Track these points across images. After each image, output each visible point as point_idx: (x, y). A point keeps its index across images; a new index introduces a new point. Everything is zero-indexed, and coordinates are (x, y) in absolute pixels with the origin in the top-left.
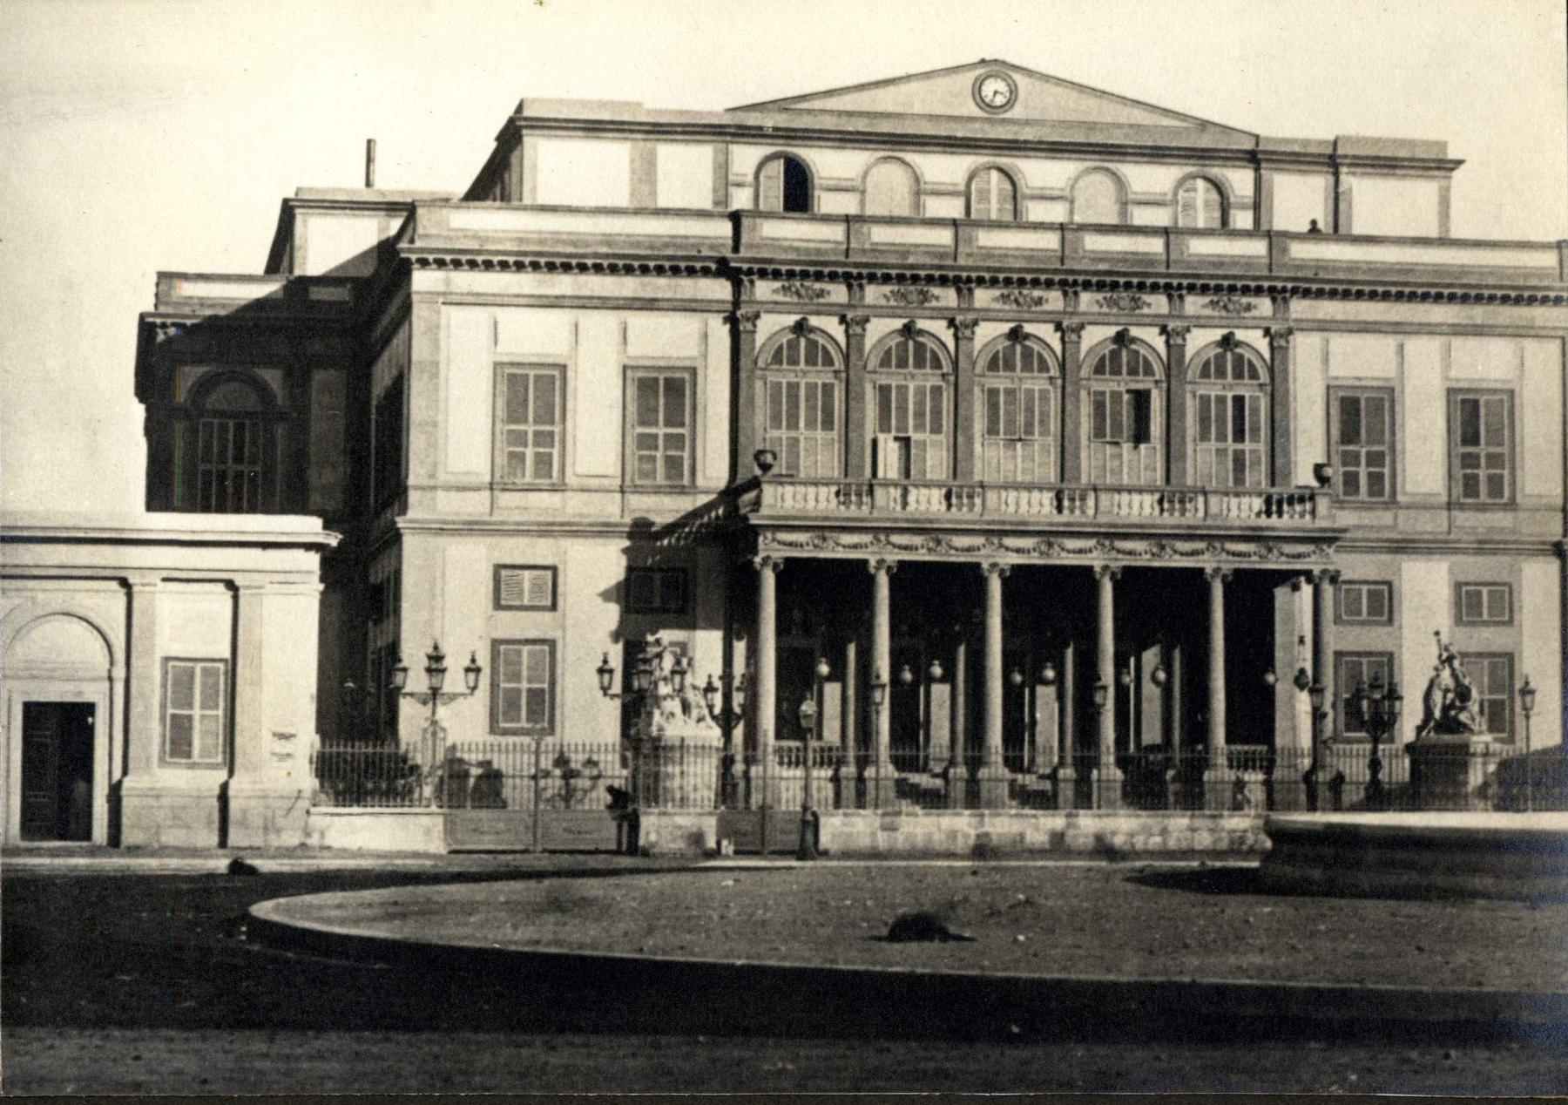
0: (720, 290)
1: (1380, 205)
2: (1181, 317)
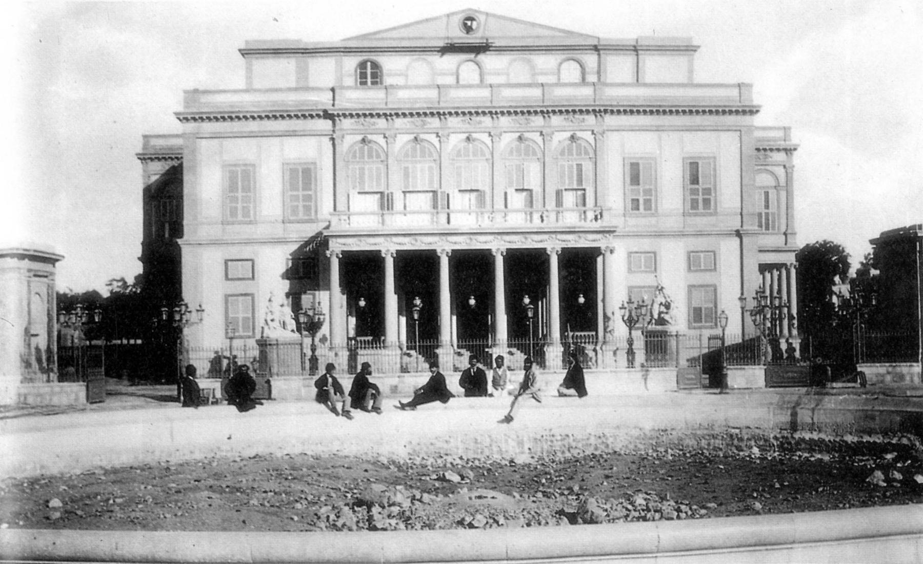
0: (326, 125)
1: (656, 68)
2: (550, 127)
